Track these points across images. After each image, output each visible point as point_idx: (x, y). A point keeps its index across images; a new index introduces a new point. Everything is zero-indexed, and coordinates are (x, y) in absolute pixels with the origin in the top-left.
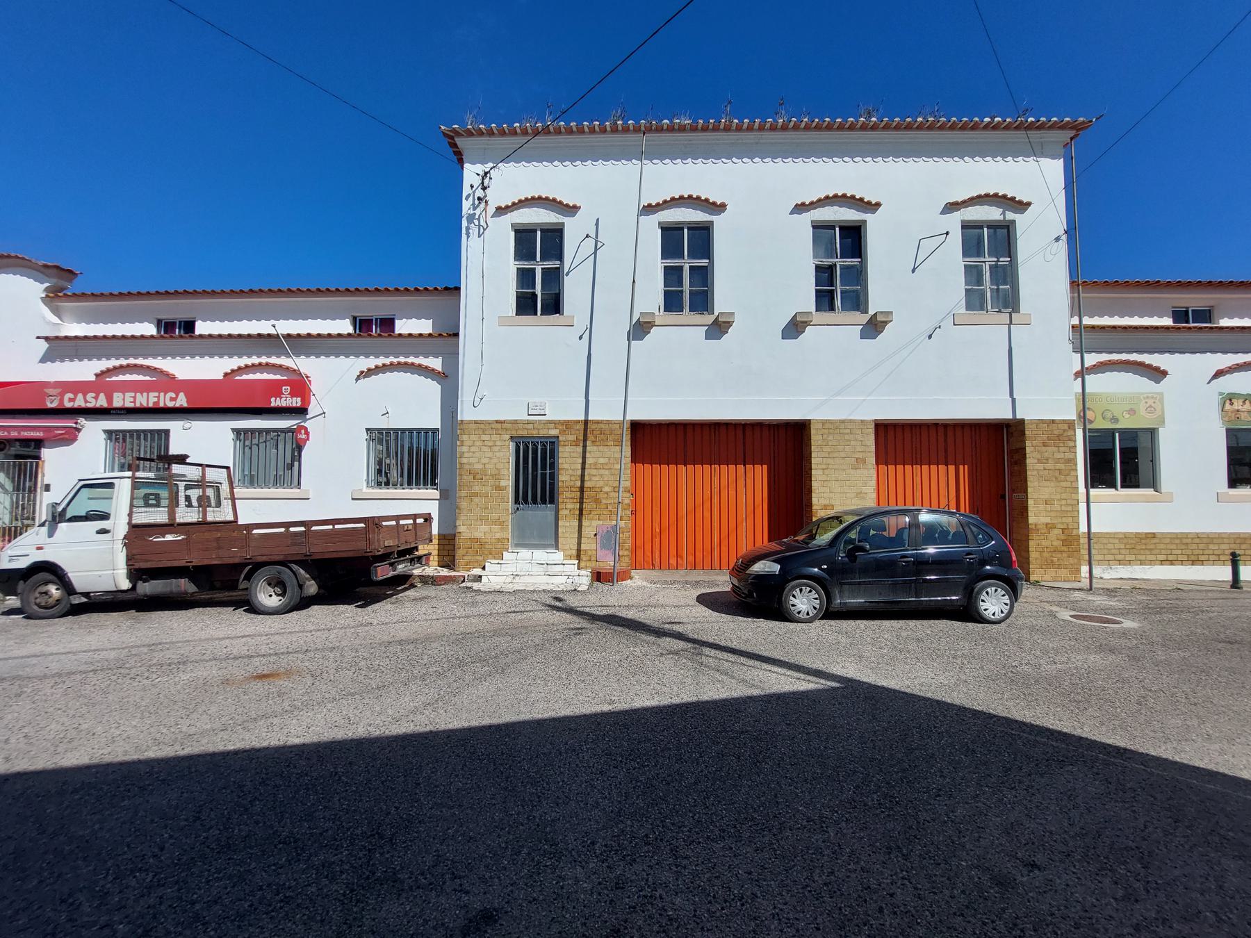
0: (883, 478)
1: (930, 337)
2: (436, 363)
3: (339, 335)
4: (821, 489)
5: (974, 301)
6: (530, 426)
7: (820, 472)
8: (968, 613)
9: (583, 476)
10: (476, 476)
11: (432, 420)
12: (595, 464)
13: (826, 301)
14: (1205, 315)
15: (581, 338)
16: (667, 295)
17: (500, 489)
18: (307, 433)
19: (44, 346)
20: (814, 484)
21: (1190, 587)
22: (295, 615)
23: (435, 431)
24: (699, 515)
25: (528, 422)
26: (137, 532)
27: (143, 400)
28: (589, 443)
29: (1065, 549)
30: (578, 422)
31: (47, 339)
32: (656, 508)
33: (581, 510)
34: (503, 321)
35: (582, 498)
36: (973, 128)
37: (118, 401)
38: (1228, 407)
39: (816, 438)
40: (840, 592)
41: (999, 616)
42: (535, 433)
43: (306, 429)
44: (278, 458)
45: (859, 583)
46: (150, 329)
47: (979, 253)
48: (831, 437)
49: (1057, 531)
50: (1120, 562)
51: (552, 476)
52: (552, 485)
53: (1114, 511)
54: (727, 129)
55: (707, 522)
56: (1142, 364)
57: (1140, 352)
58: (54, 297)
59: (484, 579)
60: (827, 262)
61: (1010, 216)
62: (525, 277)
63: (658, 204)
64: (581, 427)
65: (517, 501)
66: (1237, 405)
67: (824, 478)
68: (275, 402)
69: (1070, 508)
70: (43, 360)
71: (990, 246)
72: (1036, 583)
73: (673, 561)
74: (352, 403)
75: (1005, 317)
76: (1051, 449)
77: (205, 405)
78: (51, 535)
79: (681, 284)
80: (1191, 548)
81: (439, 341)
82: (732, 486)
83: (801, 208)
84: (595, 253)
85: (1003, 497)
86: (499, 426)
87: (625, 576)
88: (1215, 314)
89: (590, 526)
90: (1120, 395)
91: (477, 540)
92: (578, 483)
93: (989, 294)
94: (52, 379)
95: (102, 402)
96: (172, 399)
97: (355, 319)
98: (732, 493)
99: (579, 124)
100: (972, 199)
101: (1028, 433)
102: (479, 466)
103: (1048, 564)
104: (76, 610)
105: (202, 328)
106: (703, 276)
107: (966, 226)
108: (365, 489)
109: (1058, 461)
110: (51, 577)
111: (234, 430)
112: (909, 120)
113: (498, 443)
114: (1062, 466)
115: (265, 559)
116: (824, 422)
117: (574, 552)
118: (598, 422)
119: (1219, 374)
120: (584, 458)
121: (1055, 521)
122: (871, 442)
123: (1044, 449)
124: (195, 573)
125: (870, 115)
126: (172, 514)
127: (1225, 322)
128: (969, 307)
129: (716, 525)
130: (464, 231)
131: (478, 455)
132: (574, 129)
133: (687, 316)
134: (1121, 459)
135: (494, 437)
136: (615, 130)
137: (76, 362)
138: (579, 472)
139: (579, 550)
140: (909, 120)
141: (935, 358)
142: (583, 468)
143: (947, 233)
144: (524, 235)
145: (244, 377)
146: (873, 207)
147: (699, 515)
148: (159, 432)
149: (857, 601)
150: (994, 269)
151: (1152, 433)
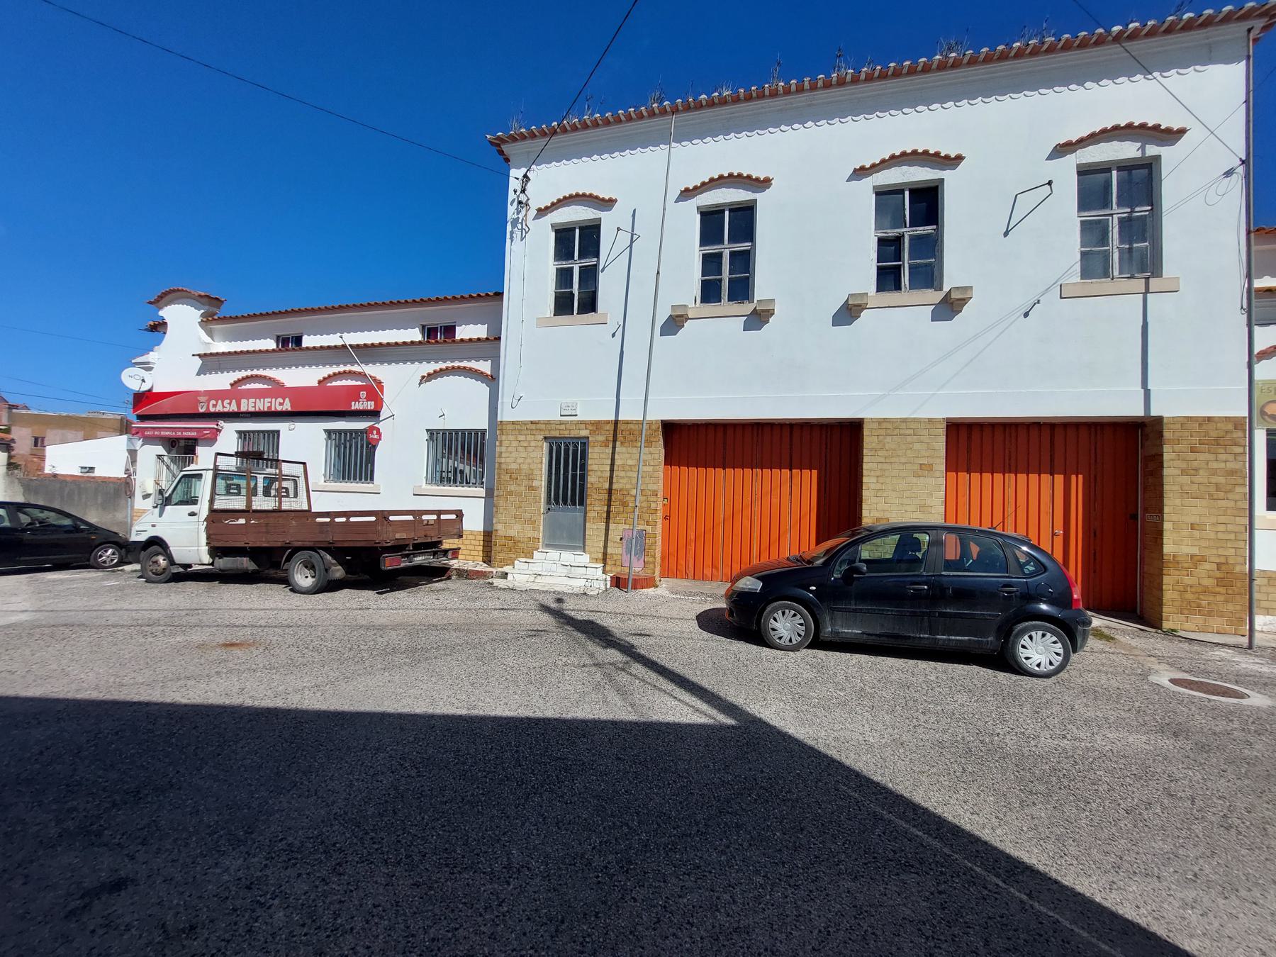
0: (964, 489)
1: (1026, 315)
2: (485, 367)
3: (412, 343)
4: (874, 500)
5: (1094, 265)
7: (874, 480)
9: (611, 477)
10: (513, 476)
11: (482, 423)
12: (623, 466)
15: (613, 335)
16: (881, 272)
17: (532, 489)
18: (379, 433)
19: (198, 362)
20: (865, 493)
22: (320, 596)
23: (483, 432)
25: (561, 423)
26: (216, 516)
27: (262, 405)
28: (618, 444)
29: (1222, 590)
30: (608, 422)
31: (199, 355)
32: (692, 514)
33: (608, 513)
34: (542, 323)
35: (610, 500)
36: (1097, 43)
37: (247, 405)
40: (831, 619)
42: (566, 433)
43: (378, 430)
44: (355, 458)
45: (855, 611)
46: (271, 344)
47: (1106, 204)
48: (889, 439)
51: (583, 478)
52: (582, 487)
54: (774, 94)
58: (208, 321)
59: (510, 577)
60: (892, 233)
61: (1152, 150)
62: (564, 277)
63: (696, 188)
64: (611, 427)
65: (549, 502)
67: (879, 486)
68: (355, 406)
69: (1232, 536)
70: (198, 374)
72: (1172, 633)
73: (708, 572)
74: (418, 403)
75: (1139, 284)
76: (1202, 457)
77: (306, 409)
78: (160, 515)
81: (487, 345)
82: (776, 492)
83: (860, 173)
84: (631, 246)
85: (1135, 517)
86: (533, 426)
87: (650, 582)
89: (617, 530)
91: (511, 538)
92: (607, 485)
93: (1116, 256)
94: (202, 389)
95: (234, 408)
96: (281, 404)
97: (423, 327)
98: (775, 501)
99: (748, 90)
100: (1092, 135)
101: (1167, 434)
102: (514, 466)
103: (1191, 608)
104: (177, 578)
105: (307, 341)
106: (744, 261)
107: (1084, 172)
108: (424, 486)
109: (1214, 472)
110: (160, 550)
111: (326, 431)
112: (1001, 47)
113: (533, 444)
114: (1222, 480)
115: (299, 544)
117: (600, 556)
118: (627, 422)
120: (613, 459)
121: (1206, 552)
122: (940, 444)
123: (1193, 456)
124: (254, 555)
125: (661, 101)
126: (249, 502)
128: (1086, 273)
131: (514, 455)
132: (611, 119)
133: (725, 306)
136: (652, 114)
137: (213, 375)
138: (608, 474)
139: (605, 554)
140: (1001, 47)
141: (1033, 338)
142: (612, 470)
143: (1050, 183)
144: (563, 236)
145: (334, 384)
146: (953, 162)
148: (273, 432)
149: (852, 631)
150: (583, 270)
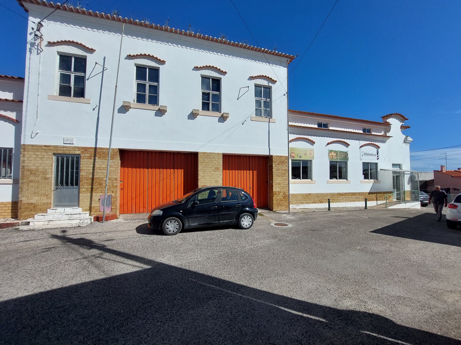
0: (228, 176)
1: (243, 124)
2: (12, 115)
5: (258, 113)
6: (65, 149)
7: (202, 173)
8: (238, 226)
9: (93, 173)
11: (10, 143)
12: (100, 167)
13: (206, 107)
14: (326, 126)
15: (94, 109)
21: (318, 211)
23: (11, 150)
24: (154, 190)
25: (64, 147)
28: (97, 158)
30: (91, 148)
34: (51, 97)
35: (92, 183)
38: (330, 154)
39: (200, 159)
41: (248, 226)
42: (67, 152)
45: (195, 217)
48: (206, 159)
49: (282, 194)
50: (301, 203)
51: (77, 173)
53: (297, 187)
55: (157, 193)
56: (344, 142)
57: (308, 135)
59: (31, 224)
60: (207, 91)
61: (270, 84)
63: (201, 67)
65: (57, 184)
66: (333, 154)
67: (203, 175)
71: (264, 93)
73: (142, 210)
76: (280, 166)
79: (209, 100)
80: (319, 198)
84: (103, 72)
85: (267, 182)
86: (46, 148)
87: (114, 217)
88: (328, 125)
89: (96, 196)
90: (301, 149)
91: (32, 204)
92: (91, 176)
98: (168, 181)
99: (176, 29)
103: (279, 205)
106: (155, 90)
114: (284, 172)
116: (204, 153)
117: (88, 208)
118: (101, 149)
119: (328, 144)
121: (281, 190)
122: (221, 161)
127: (331, 128)
128: (203, 109)
129: (161, 194)
130: (28, 50)
133: (147, 105)
134: (302, 170)
135: (43, 153)
138: (92, 171)
139: (90, 207)
142: (94, 169)
147: (154, 190)
149: (194, 224)
151: (311, 161)
